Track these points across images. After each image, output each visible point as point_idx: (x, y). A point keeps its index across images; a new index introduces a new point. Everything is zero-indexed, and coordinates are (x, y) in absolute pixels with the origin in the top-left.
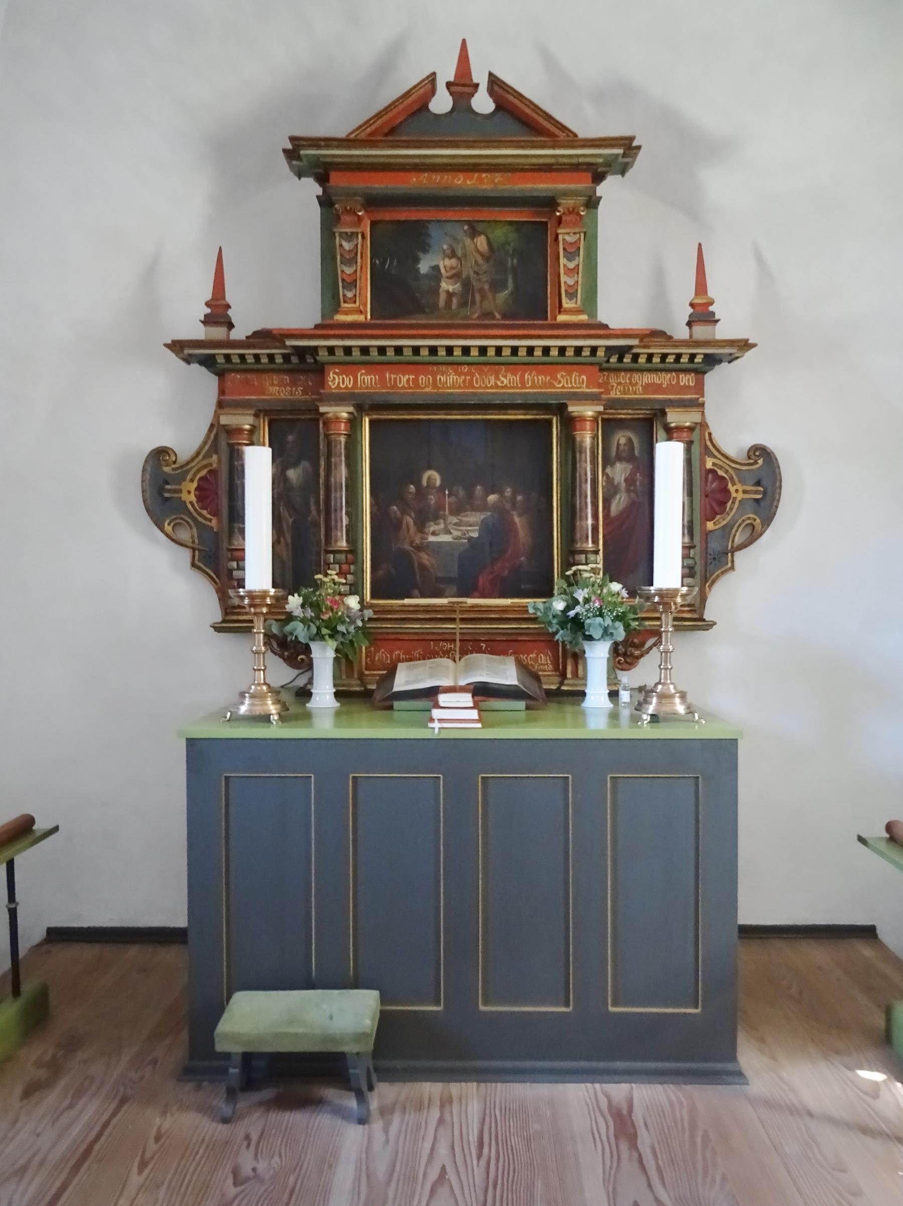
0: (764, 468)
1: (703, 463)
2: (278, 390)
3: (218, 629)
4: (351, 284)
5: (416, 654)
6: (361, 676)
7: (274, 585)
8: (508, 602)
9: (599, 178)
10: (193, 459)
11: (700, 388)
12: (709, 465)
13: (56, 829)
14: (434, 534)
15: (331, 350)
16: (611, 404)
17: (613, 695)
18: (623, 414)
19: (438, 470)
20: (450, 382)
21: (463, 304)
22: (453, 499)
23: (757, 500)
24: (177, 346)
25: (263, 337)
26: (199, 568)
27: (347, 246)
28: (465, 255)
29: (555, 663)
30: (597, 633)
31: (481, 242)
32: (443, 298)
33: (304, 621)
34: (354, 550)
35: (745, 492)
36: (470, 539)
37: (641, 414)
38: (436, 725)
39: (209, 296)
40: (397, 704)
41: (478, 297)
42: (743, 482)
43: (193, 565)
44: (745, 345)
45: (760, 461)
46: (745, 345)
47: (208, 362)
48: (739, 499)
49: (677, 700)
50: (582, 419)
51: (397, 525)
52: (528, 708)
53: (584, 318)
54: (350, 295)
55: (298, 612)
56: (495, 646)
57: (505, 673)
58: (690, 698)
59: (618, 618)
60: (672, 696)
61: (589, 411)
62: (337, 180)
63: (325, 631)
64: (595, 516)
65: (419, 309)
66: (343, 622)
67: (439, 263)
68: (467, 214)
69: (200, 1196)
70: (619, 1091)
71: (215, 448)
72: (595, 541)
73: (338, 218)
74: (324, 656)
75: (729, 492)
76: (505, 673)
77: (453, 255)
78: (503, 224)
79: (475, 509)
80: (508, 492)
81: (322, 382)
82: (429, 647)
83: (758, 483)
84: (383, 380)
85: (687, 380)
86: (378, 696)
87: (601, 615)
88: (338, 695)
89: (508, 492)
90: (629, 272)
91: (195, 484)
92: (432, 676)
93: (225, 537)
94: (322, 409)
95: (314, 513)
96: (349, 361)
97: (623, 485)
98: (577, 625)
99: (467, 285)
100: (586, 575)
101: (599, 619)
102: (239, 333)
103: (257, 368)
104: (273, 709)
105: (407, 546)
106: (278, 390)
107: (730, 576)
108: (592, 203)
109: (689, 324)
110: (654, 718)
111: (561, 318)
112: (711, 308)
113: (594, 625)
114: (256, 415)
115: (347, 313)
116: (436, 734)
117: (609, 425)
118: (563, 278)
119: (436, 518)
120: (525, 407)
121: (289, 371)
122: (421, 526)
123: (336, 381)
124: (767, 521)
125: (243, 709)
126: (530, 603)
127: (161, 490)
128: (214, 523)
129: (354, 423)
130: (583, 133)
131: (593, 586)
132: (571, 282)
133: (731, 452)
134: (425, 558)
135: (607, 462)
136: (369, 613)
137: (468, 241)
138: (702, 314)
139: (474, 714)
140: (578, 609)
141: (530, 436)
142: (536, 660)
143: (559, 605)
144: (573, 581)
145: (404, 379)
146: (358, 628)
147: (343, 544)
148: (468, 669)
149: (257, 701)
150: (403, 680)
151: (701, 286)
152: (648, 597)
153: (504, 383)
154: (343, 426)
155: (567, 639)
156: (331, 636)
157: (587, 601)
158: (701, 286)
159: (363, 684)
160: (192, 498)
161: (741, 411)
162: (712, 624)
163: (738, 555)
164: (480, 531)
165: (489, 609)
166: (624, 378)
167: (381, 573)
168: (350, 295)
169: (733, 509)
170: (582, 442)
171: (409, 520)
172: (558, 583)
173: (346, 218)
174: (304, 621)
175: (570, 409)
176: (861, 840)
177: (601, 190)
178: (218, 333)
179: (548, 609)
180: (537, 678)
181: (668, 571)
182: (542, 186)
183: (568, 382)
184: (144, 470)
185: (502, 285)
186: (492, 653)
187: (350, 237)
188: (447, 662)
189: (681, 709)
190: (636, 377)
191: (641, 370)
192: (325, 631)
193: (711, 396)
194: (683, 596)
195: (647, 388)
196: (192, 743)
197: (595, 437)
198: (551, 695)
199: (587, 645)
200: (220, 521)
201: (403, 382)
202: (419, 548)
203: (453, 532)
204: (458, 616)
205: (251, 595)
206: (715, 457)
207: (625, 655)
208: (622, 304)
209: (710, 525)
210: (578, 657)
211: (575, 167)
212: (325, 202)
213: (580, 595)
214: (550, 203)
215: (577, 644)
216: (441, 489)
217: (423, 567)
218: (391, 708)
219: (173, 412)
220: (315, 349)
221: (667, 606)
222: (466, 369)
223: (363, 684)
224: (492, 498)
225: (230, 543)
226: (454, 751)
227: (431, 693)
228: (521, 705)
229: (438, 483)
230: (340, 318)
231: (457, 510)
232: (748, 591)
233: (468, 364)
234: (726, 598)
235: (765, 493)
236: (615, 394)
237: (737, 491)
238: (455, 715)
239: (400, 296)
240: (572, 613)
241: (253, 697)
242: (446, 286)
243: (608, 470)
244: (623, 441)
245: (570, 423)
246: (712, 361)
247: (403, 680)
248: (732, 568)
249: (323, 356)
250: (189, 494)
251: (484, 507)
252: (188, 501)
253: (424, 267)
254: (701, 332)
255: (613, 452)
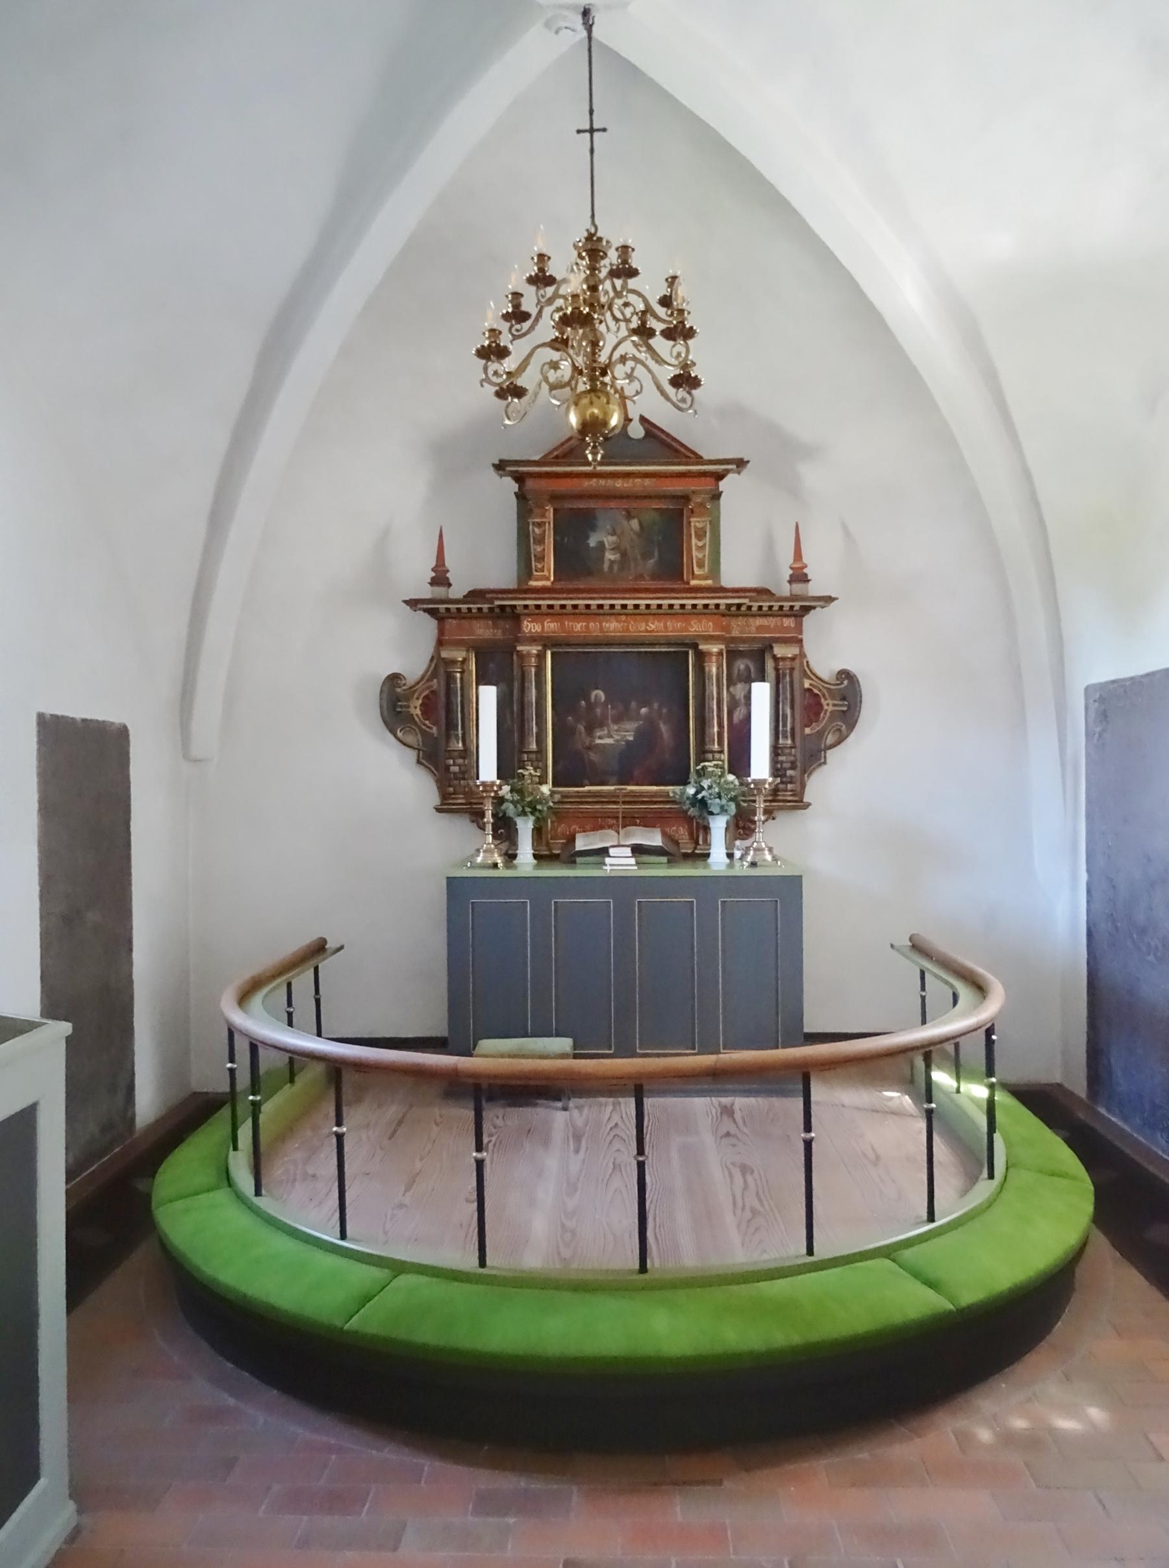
0: (848, 690)
1: (802, 684)
2: (483, 631)
3: (439, 810)
4: (541, 558)
5: (588, 827)
6: (548, 844)
7: (498, 778)
8: (655, 788)
9: (720, 477)
10: (418, 683)
11: (799, 628)
12: (807, 685)
13: (342, 948)
14: (600, 738)
15: (526, 607)
16: (734, 640)
17: (730, 856)
18: (742, 647)
19: (604, 691)
20: (613, 627)
21: (622, 569)
22: (614, 711)
23: (843, 711)
24: (413, 603)
25: (475, 595)
26: (422, 764)
27: (537, 530)
28: (623, 533)
29: (691, 834)
30: (716, 810)
31: (635, 524)
32: (606, 566)
33: (512, 802)
34: (541, 751)
35: (834, 705)
36: (628, 742)
37: (756, 646)
38: (608, 868)
39: (433, 564)
40: (579, 860)
41: (632, 564)
42: (833, 698)
43: (419, 762)
44: (829, 600)
45: (846, 682)
46: (829, 600)
47: (432, 613)
48: (823, 713)
49: (767, 852)
50: (710, 654)
51: (573, 731)
52: (669, 862)
53: (709, 582)
54: (540, 566)
55: (509, 796)
56: (647, 821)
57: (654, 839)
58: (775, 852)
59: (731, 799)
60: (763, 850)
61: (715, 649)
62: (530, 484)
63: (528, 809)
64: (720, 725)
65: (590, 573)
66: (541, 803)
67: (601, 537)
68: (625, 504)
69: (627, 799)
70: (725, 1100)
71: (435, 675)
72: (720, 743)
73: (531, 511)
74: (525, 827)
75: (821, 705)
76: (654, 839)
77: (614, 533)
78: (650, 511)
79: (630, 719)
80: (656, 706)
81: (518, 627)
82: (598, 822)
83: (844, 699)
84: (563, 625)
85: (789, 622)
86: (563, 857)
87: (720, 797)
88: (535, 856)
89: (656, 706)
90: (743, 547)
91: (420, 701)
92: (601, 841)
93: (443, 742)
94: (519, 648)
95: (509, 722)
96: (538, 613)
97: (743, 700)
98: (703, 803)
99: (624, 555)
100: (710, 769)
101: (717, 800)
102: (458, 590)
103: (469, 616)
104: (499, 860)
105: (579, 747)
106: (483, 631)
107: (824, 767)
108: (716, 496)
109: (790, 582)
110: (753, 864)
111: (694, 583)
112: (805, 571)
113: (714, 805)
114: (468, 651)
115: (537, 580)
116: (608, 873)
117: (733, 655)
118: (695, 553)
119: (601, 725)
120: (669, 644)
121: (491, 618)
122: (590, 730)
123: (530, 627)
124: (851, 726)
125: (479, 859)
126: (677, 789)
127: (394, 706)
128: (435, 730)
129: (541, 657)
130: (706, 457)
131: (712, 779)
132: (700, 556)
133: (825, 675)
134: (593, 756)
135: (731, 682)
136: (557, 797)
137: (625, 522)
138: (798, 576)
139: (632, 861)
140: (704, 793)
141: (673, 664)
142: (677, 831)
143: (691, 791)
144: (702, 774)
145: (579, 626)
146: (550, 808)
147: (534, 747)
148: (627, 836)
149: (488, 855)
150: (581, 844)
151: (798, 555)
152: (748, 784)
153: (655, 627)
154: (533, 660)
155: (697, 814)
156: (532, 813)
157: (710, 787)
158: (798, 555)
159: (550, 850)
160: (418, 712)
161: (828, 648)
162: (809, 805)
163: (829, 752)
164: (635, 737)
165: (642, 794)
166: (741, 621)
167: (559, 767)
168: (540, 566)
169: (825, 718)
170: (710, 671)
171: (581, 727)
172: (693, 777)
173: (536, 511)
174: (512, 802)
175: (701, 647)
176: (892, 946)
177: (723, 485)
178: (440, 592)
179: (683, 793)
180: (677, 843)
181: (760, 767)
182: (677, 487)
183: (697, 627)
184: (381, 691)
185: (651, 556)
186: (645, 826)
187: (539, 525)
188: (612, 832)
189: (769, 857)
190: (751, 620)
191: (754, 616)
192: (528, 809)
193: (807, 636)
194: (770, 784)
195: (760, 628)
196: (450, 880)
197: (719, 667)
198: (686, 856)
199: (710, 818)
200: (439, 730)
201: (578, 627)
202: (589, 748)
203: (613, 737)
204: (621, 800)
205: (484, 784)
206: (810, 678)
207: (744, 828)
208: (740, 566)
209: (808, 731)
210: (707, 829)
211: (704, 474)
212: (521, 496)
213: (706, 783)
214: (686, 498)
215: (704, 818)
216: (606, 704)
217: (590, 761)
218: (574, 862)
219: (406, 650)
220: (514, 607)
221: (759, 790)
222: (623, 618)
223: (550, 850)
224: (644, 710)
225: (447, 746)
226: (619, 884)
227: (604, 852)
228: (664, 859)
229: (603, 698)
230: (533, 583)
231: (618, 720)
232: (838, 780)
233: (626, 615)
234: (822, 786)
235: (849, 706)
236: (735, 633)
237: (829, 705)
238: (621, 861)
239: (575, 562)
240: (699, 796)
241: (485, 851)
242: (610, 556)
243: (731, 689)
244: (742, 667)
245: (701, 657)
246: (806, 610)
247: (581, 844)
248: (825, 763)
249: (519, 610)
250: (416, 710)
251: (638, 717)
252: (422, 716)
253: (592, 542)
254: (798, 588)
255: (735, 676)
